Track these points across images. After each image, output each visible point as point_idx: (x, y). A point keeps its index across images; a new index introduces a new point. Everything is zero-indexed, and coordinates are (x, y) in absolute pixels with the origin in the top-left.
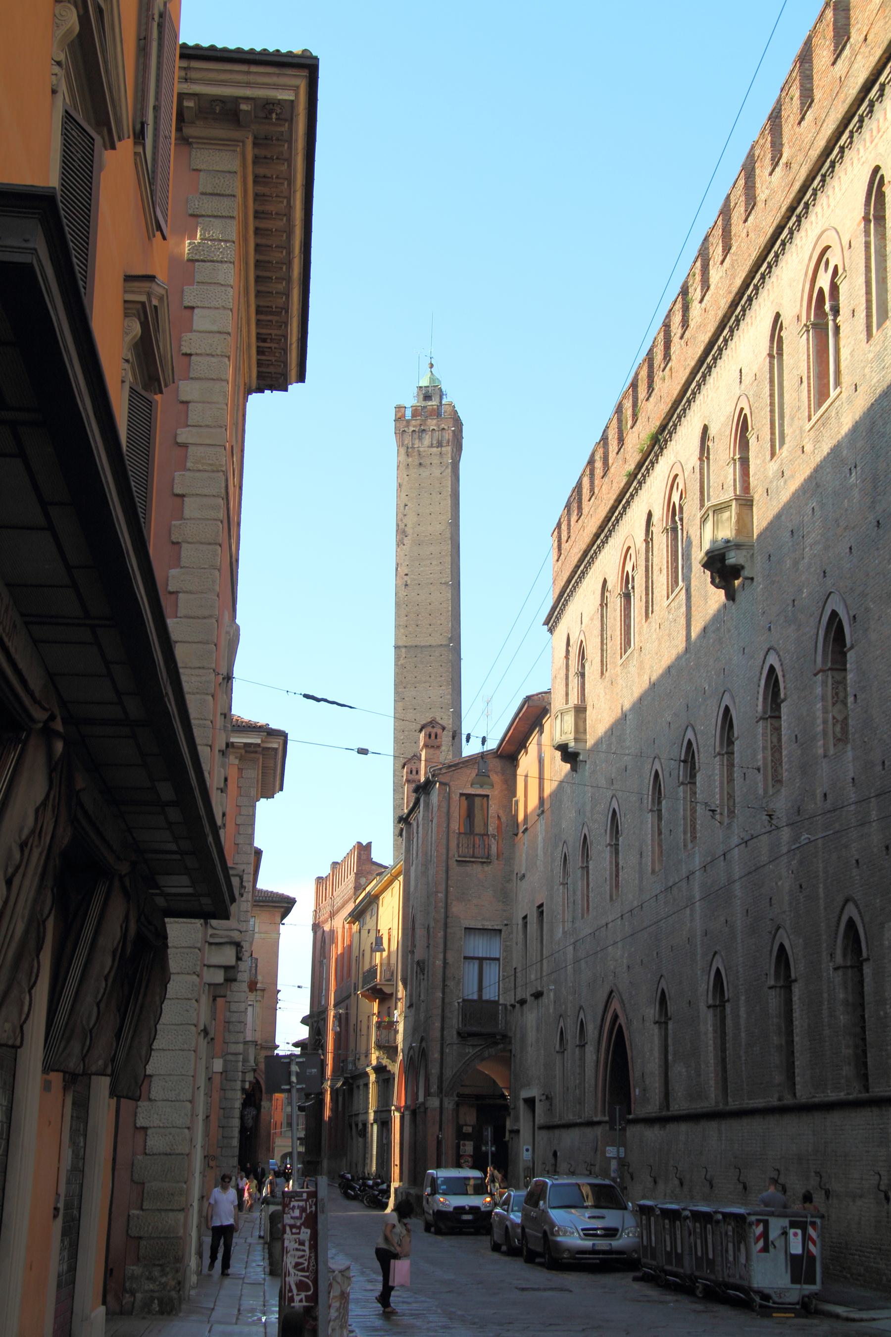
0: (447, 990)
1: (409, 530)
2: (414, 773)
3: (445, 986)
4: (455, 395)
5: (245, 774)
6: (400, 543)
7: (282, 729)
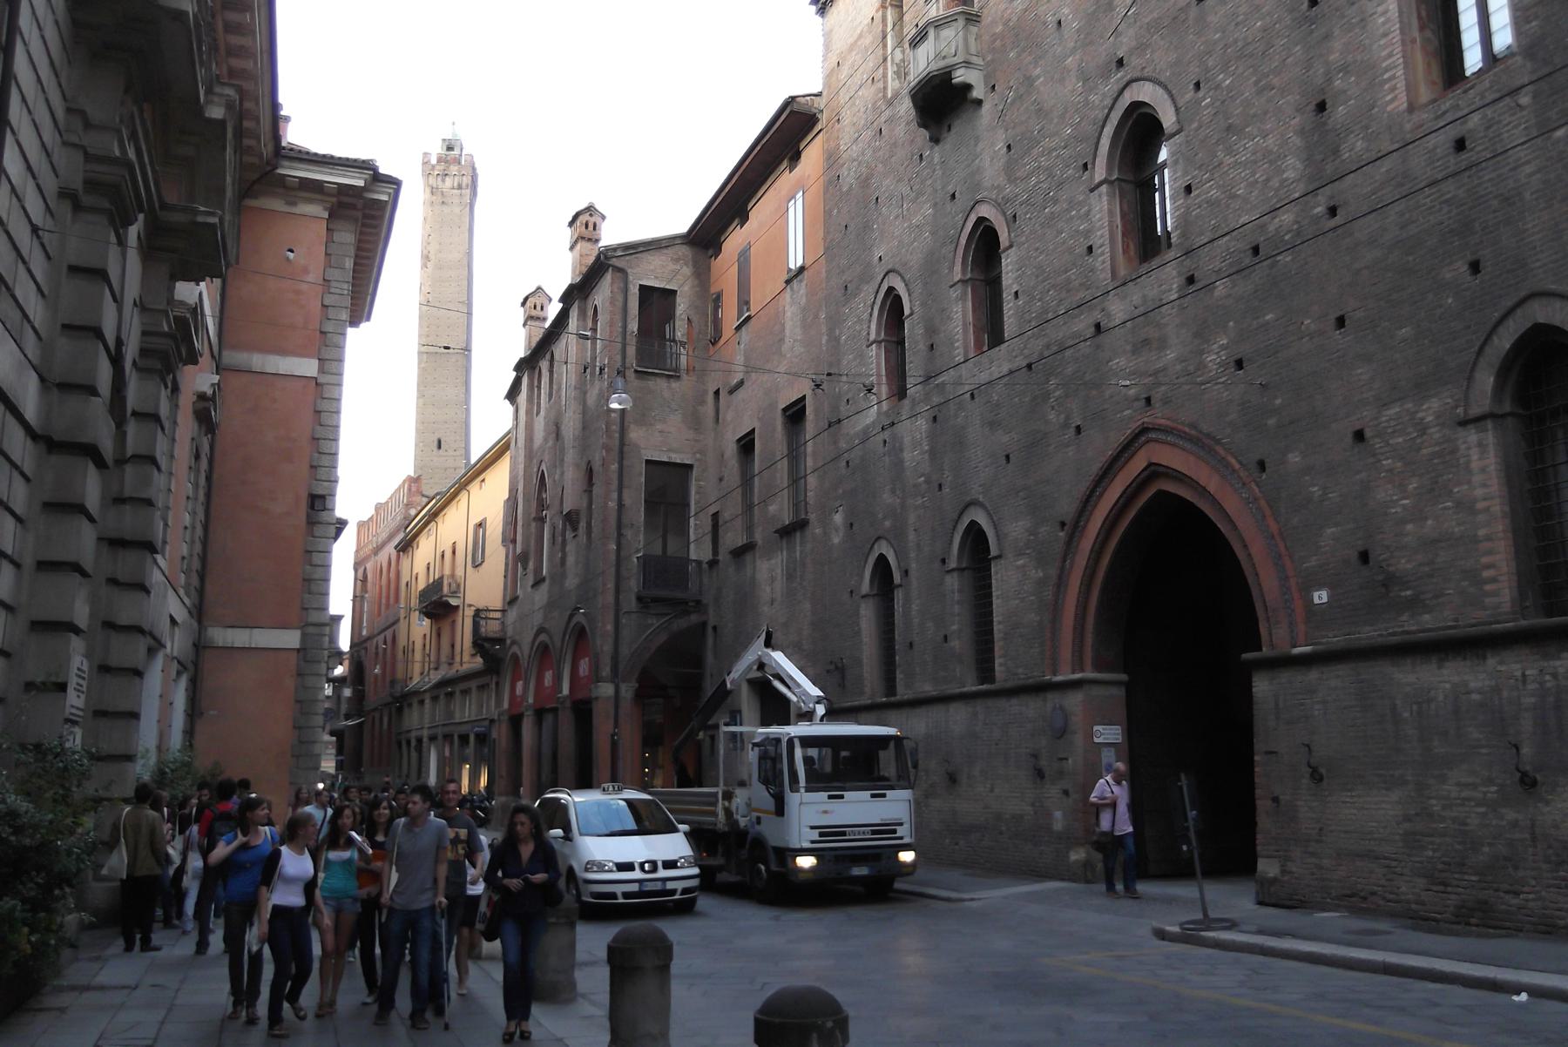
0: (623, 541)
1: (432, 256)
2: (591, 227)
3: (620, 535)
4: (471, 147)
5: (337, 237)
6: (424, 266)
7: (394, 175)
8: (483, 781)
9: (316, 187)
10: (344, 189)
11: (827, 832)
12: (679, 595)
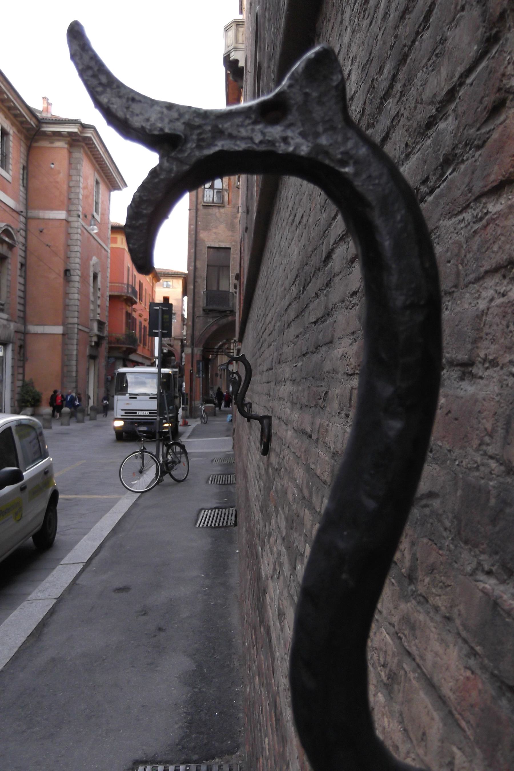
0: (197, 284)
8: (231, 389)
9: (58, 134)
10: (70, 134)
11: (128, 412)
12: (225, 308)
